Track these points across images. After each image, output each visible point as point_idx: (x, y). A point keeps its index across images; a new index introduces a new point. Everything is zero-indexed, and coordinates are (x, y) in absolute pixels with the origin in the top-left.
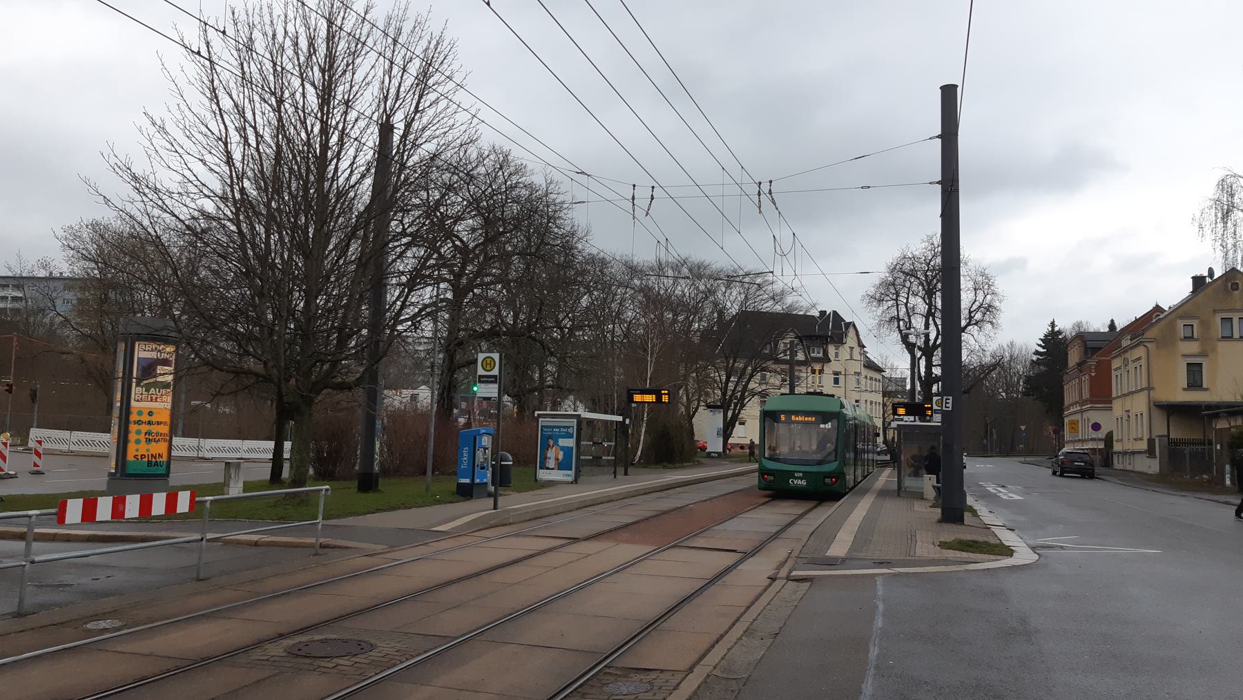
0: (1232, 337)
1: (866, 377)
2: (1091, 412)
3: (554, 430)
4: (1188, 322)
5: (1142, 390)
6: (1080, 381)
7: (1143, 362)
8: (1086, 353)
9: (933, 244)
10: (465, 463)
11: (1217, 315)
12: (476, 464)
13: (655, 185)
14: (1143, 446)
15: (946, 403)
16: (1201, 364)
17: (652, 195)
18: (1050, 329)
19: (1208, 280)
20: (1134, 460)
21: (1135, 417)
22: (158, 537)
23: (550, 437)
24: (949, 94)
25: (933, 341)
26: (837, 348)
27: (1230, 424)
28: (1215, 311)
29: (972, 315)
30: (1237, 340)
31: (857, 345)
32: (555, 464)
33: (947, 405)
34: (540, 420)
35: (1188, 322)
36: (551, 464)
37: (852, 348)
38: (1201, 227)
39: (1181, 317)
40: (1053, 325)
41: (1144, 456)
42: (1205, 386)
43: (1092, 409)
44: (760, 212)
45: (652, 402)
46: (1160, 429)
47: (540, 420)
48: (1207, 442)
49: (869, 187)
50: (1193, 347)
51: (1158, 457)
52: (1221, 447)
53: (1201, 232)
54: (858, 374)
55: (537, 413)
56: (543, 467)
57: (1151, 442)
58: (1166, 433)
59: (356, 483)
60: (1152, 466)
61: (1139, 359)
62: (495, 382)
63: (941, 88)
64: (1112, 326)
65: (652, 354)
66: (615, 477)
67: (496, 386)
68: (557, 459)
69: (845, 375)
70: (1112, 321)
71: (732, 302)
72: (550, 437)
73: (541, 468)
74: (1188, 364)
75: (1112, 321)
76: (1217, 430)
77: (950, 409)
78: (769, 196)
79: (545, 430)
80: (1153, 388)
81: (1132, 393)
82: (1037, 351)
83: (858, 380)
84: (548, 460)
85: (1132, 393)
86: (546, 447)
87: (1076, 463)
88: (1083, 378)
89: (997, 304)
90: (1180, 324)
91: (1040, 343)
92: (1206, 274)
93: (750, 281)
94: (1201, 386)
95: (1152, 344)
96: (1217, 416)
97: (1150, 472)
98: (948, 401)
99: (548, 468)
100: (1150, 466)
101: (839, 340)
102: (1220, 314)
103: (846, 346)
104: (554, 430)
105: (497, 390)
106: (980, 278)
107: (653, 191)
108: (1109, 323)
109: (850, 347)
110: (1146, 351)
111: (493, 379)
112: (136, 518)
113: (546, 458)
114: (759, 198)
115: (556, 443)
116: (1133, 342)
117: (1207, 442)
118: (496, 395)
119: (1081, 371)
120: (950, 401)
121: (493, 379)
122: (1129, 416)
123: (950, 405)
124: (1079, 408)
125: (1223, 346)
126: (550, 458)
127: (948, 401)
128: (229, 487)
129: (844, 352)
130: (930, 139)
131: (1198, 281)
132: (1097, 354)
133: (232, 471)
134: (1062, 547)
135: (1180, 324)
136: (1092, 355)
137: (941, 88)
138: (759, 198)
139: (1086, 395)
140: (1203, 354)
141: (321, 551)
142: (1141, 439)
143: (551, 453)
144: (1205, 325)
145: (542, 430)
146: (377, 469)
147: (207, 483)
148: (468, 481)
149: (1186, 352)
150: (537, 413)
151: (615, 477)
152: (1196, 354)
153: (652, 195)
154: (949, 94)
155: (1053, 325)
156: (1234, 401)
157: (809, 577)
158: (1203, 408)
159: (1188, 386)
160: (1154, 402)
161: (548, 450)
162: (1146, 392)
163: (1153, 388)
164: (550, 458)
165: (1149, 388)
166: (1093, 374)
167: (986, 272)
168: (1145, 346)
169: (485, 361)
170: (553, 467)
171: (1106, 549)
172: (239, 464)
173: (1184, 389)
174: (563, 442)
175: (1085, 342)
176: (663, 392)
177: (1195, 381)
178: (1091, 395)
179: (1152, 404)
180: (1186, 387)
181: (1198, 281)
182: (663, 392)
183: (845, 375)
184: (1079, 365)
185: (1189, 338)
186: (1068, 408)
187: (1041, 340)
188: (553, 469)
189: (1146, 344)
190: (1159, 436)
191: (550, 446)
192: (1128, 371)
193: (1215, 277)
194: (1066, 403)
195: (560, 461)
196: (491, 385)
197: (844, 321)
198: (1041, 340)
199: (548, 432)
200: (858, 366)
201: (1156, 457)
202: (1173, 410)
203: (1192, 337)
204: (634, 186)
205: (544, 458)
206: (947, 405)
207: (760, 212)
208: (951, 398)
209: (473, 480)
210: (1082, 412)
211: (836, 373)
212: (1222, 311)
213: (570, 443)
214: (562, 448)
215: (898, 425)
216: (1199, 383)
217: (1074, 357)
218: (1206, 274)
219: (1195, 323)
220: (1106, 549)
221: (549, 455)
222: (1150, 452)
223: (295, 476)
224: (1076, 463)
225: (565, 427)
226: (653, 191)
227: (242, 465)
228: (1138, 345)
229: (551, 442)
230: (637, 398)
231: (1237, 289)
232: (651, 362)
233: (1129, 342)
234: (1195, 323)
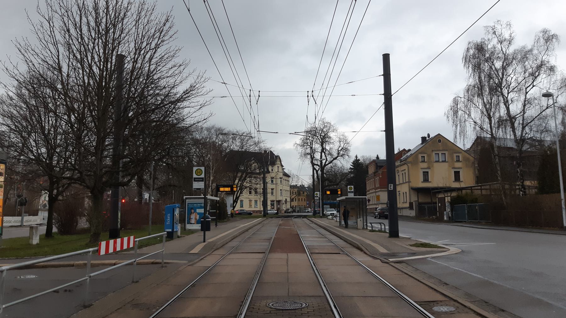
0: (439, 161)
1: (284, 179)
2: (380, 192)
3: (194, 205)
4: (458, 155)
5: (406, 182)
6: (375, 181)
7: (406, 171)
8: (377, 168)
9: (324, 122)
10: (169, 222)
11: (433, 152)
12: (174, 222)
13: (251, 90)
14: (407, 205)
15: (390, 187)
16: (428, 172)
17: (259, 95)
18: (355, 158)
19: (427, 138)
20: (402, 211)
21: (402, 194)
22: (442, 247)
23: (192, 209)
24: (386, 58)
25: (324, 163)
26: (273, 167)
27: (445, 196)
28: (432, 151)
29: (339, 152)
30: (441, 162)
31: (280, 165)
32: (195, 222)
33: (391, 188)
34: (187, 200)
35: (423, 155)
36: (193, 221)
37: (278, 167)
38: (448, 117)
39: (421, 153)
40: (356, 157)
41: (408, 210)
42: (429, 181)
43: (380, 191)
44: (257, 104)
45: (229, 191)
46: (414, 198)
47: (187, 200)
48: (432, 203)
49: (352, 95)
50: (425, 165)
51: (414, 209)
52: (441, 205)
53: (448, 119)
54: (281, 178)
55: (185, 197)
56: (189, 223)
57: (411, 204)
58: (417, 200)
59: (108, 233)
60: (413, 213)
61: (405, 170)
62: (203, 181)
63: (383, 55)
64: (378, 157)
65: (212, 169)
66: (216, 227)
67: (203, 183)
68: (196, 219)
69: (276, 179)
70: (377, 155)
71: (235, 146)
72: (192, 209)
73: (188, 223)
74: (454, 171)
75: (377, 155)
76: (439, 198)
77: (392, 189)
78: (249, 97)
79: (189, 205)
80: (411, 182)
81: (401, 184)
82: (350, 168)
83: (281, 180)
84: (191, 219)
85: (401, 184)
86: (190, 213)
87: (385, 213)
88: (376, 179)
89: (349, 148)
90: (420, 156)
91: (352, 164)
92: (426, 136)
93: (245, 137)
94: (428, 180)
95: (409, 164)
96: (440, 192)
97: (411, 215)
98: (391, 186)
99: (191, 224)
100: (411, 213)
101: (273, 164)
102: (435, 152)
103: (276, 166)
104: (194, 205)
105: (204, 185)
106: (342, 137)
107: (259, 93)
108: (376, 156)
109: (277, 167)
110: (407, 167)
111: (202, 180)
112: (112, 253)
113: (190, 219)
114: (313, 98)
115: (195, 211)
116: (401, 163)
117: (432, 203)
118: (203, 187)
119: (375, 176)
120: (392, 186)
121: (202, 180)
122: (400, 194)
123: (392, 188)
124: (375, 191)
125: (436, 165)
126: (192, 219)
127: (391, 186)
128: (32, 239)
129: (275, 169)
130: (379, 76)
131: (424, 139)
132: (382, 168)
133: (34, 231)
134: (452, 244)
135: (420, 156)
136: (380, 169)
137: (383, 55)
138: (313, 98)
139: (378, 185)
140: (429, 168)
141: (164, 265)
142: (406, 202)
143: (193, 216)
144: (429, 156)
145: (188, 205)
146: (119, 226)
147: (8, 238)
148: (170, 230)
149: (423, 167)
150: (185, 197)
151: (216, 227)
152: (426, 168)
153: (259, 95)
154: (386, 58)
155: (356, 157)
156: (437, 186)
157: (401, 261)
158: (431, 189)
159: (424, 181)
160: (411, 187)
161: (191, 215)
162: (408, 183)
163: (411, 182)
164: (192, 219)
165: (409, 182)
166: (381, 177)
167: (345, 134)
168: (407, 165)
169: (201, 173)
170: (194, 223)
171: (461, 244)
172: (37, 227)
173: (422, 182)
174: (198, 211)
175: (376, 163)
176: (234, 186)
177: (426, 180)
178: (380, 184)
179: (410, 188)
180: (423, 181)
181: (424, 139)
182: (234, 186)
183: (276, 179)
184: (374, 173)
185: (423, 161)
186: (369, 191)
187: (352, 163)
188: (194, 224)
189: (408, 164)
190: (415, 201)
191: (192, 213)
192: (399, 175)
193: (430, 137)
194: (368, 189)
195: (197, 220)
196: (200, 183)
197: (275, 155)
198: (352, 163)
199: (191, 206)
200: (281, 175)
201: (414, 210)
202: (419, 191)
203: (445, 161)
204: (259, 91)
205: (190, 219)
206: (391, 188)
207: (257, 104)
208: (392, 185)
209: (173, 229)
210: (376, 192)
211: (272, 178)
212: (435, 151)
213: (202, 211)
214: (198, 214)
215: (346, 198)
216: (427, 179)
217: (371, 170)
218: (426, 136)
219: (425, 155)
220: (461, 244)
221: (191, 217)
222: (411, 207)
223: (95, 231)
224: (385, 213)
225: (195, 204)
226: (259, 93)
227: (39, 227)
228: (404, 164)
229: (193, 211)
230: (222, 189)
231: (440, 142)
232: (212, 173)
233: (399, 163)
234: (425, 155)
